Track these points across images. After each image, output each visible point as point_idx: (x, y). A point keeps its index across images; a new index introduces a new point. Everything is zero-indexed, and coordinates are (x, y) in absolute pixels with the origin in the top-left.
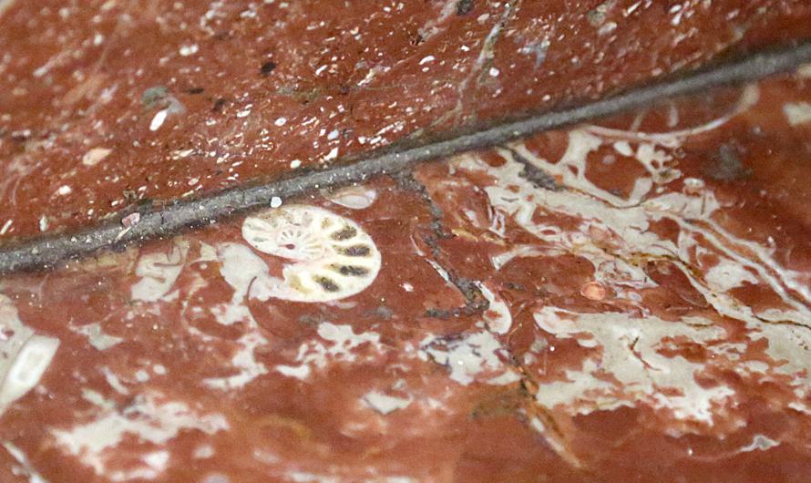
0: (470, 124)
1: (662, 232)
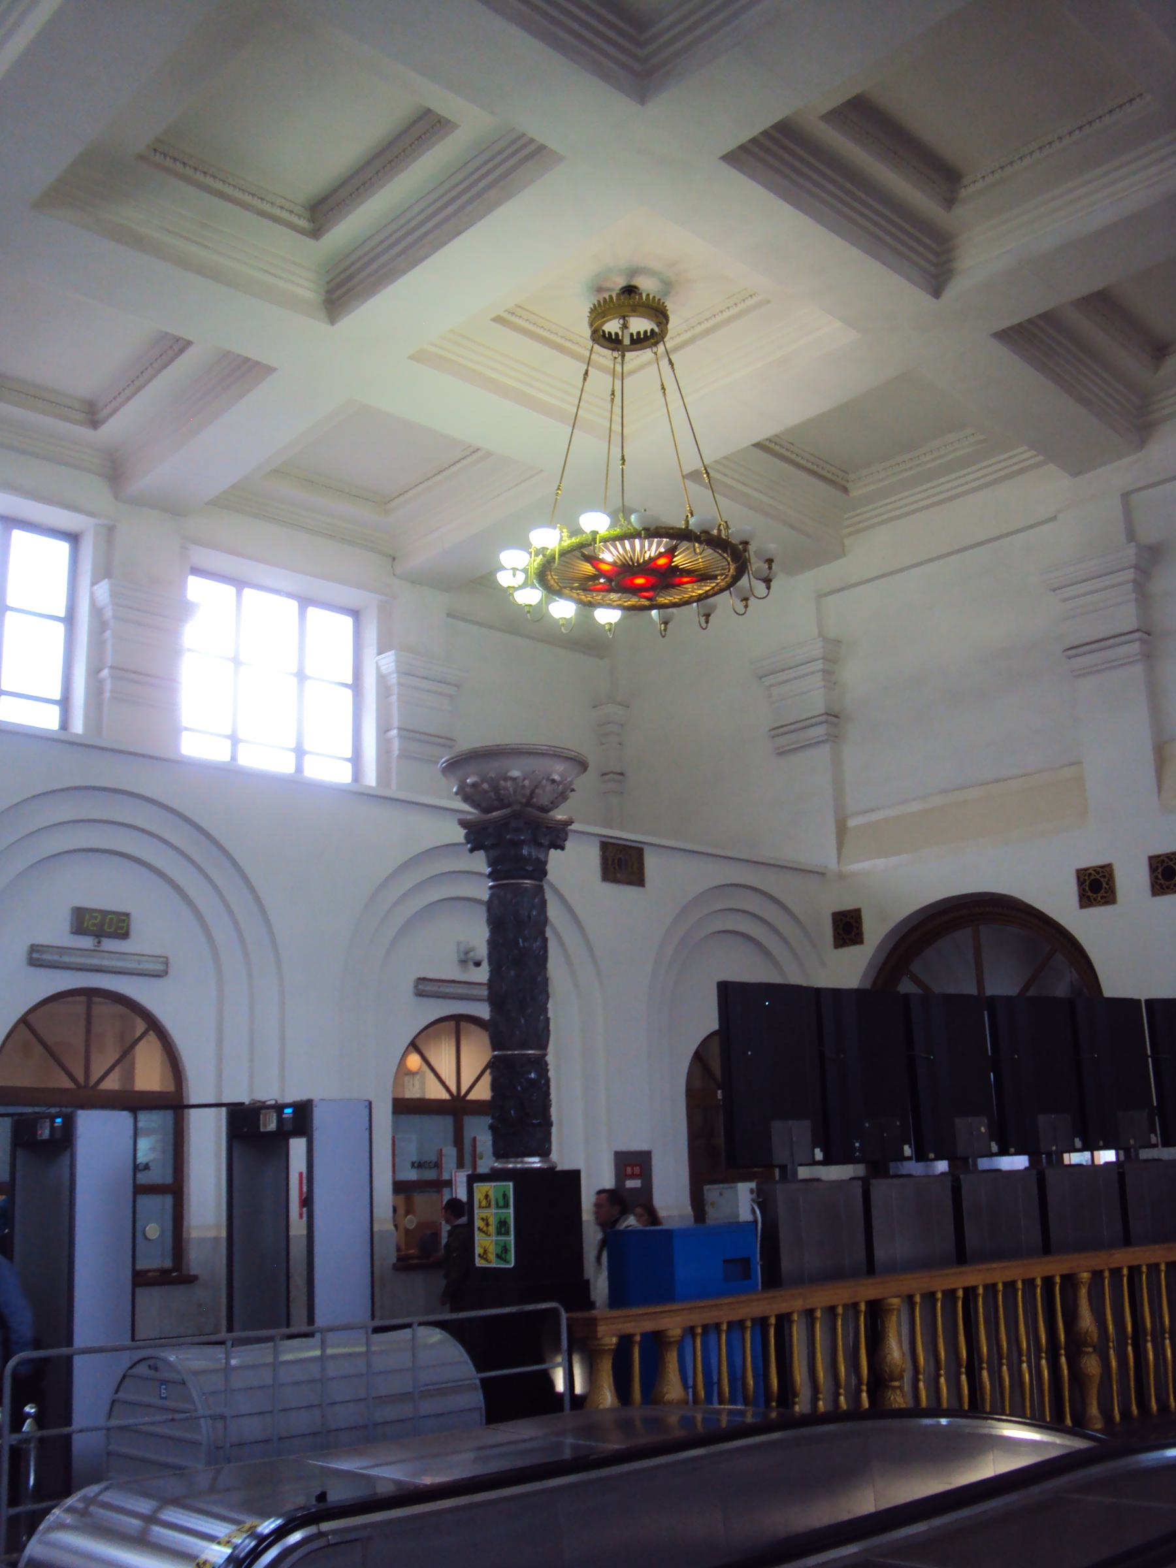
0: (473, 838)
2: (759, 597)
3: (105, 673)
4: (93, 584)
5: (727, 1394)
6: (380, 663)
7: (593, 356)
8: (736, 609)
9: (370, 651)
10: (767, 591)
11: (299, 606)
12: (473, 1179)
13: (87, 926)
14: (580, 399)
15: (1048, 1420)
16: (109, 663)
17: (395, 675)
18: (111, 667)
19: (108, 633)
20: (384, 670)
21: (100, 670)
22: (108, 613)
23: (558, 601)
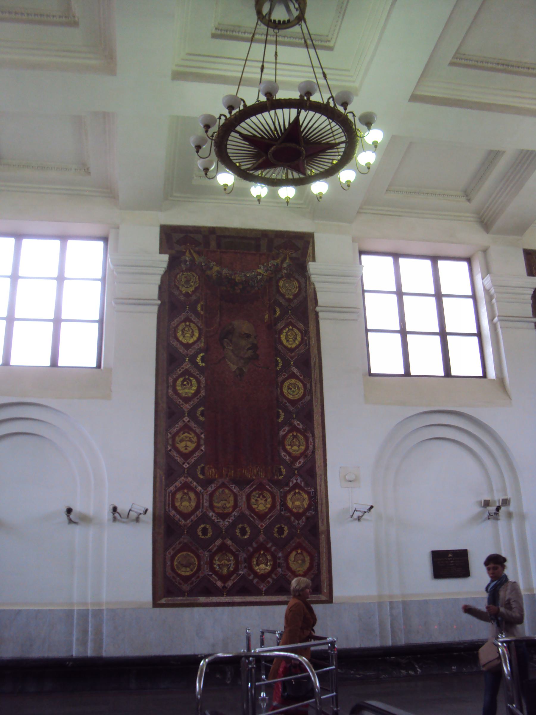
2: (206, 157)
3: (496, 319)
4: (483, 279)
5: (457, 653)
6: (485, 283)
7: (278, 39)
8: (361, 172)
9: (478, 278)
10: (375, 149)
11: (393, 259)
12: (221, 476)
13: (203, 378)
14: (276, 75)
15: (257, 684)
16: (497, 315)
17: (493, 288)
18: (498, 316)
19: (494, 301)
20: (487, 287)
21: (494, 318)
22: (492, 291)
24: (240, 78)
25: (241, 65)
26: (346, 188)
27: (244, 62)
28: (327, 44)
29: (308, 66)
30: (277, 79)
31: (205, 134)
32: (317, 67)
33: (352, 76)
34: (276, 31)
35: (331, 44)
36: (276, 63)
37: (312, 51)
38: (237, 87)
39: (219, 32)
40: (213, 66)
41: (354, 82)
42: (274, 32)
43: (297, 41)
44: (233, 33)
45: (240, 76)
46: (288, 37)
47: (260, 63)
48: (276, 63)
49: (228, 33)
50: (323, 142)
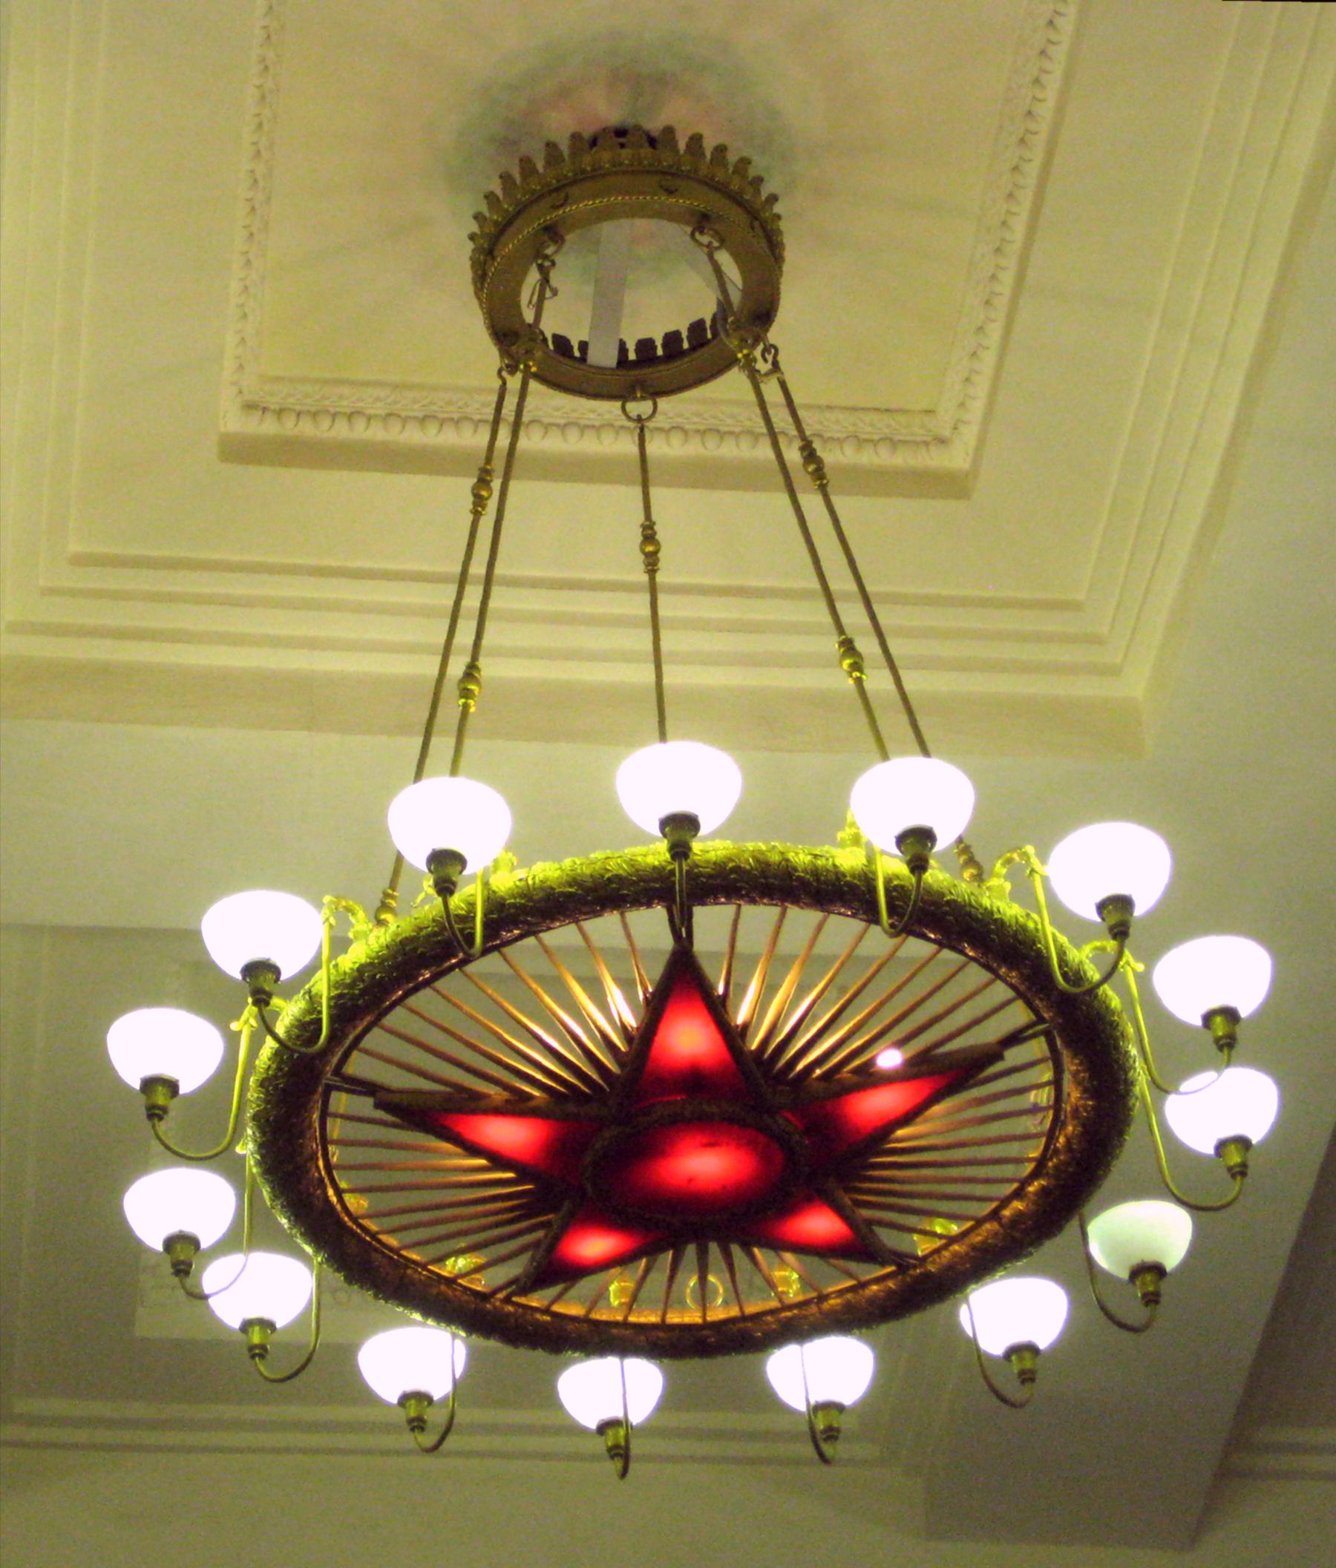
1: (335, 1266)
23: (312, 1275)
24: (433, 684)
25: (427, 612)
26: (1014, 1390)
27: (452, 590)
28: (935, 459)
29: (805, 595)
30: (667, 680)
31: (1045, 874)
32: (847, 596)
33: (1095, 640)
34: (640, 407)
35: (956, 459)
36: (653, 589)
37: (812, 503)
38: (419, 741)
39: (269, 427)
40: (239, 622)
41: (1113, 671)
42: (629, 418)
43: (729, 450)
44: (351, 428)
45: (435, 671)
46: (685, 432)
47: (442, 586)
48: (653, 589)
49: (290, 422)
50: (510, 1175)
